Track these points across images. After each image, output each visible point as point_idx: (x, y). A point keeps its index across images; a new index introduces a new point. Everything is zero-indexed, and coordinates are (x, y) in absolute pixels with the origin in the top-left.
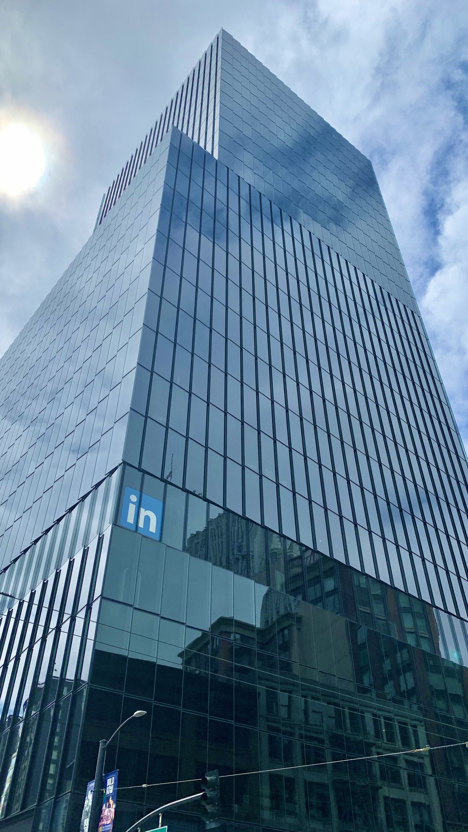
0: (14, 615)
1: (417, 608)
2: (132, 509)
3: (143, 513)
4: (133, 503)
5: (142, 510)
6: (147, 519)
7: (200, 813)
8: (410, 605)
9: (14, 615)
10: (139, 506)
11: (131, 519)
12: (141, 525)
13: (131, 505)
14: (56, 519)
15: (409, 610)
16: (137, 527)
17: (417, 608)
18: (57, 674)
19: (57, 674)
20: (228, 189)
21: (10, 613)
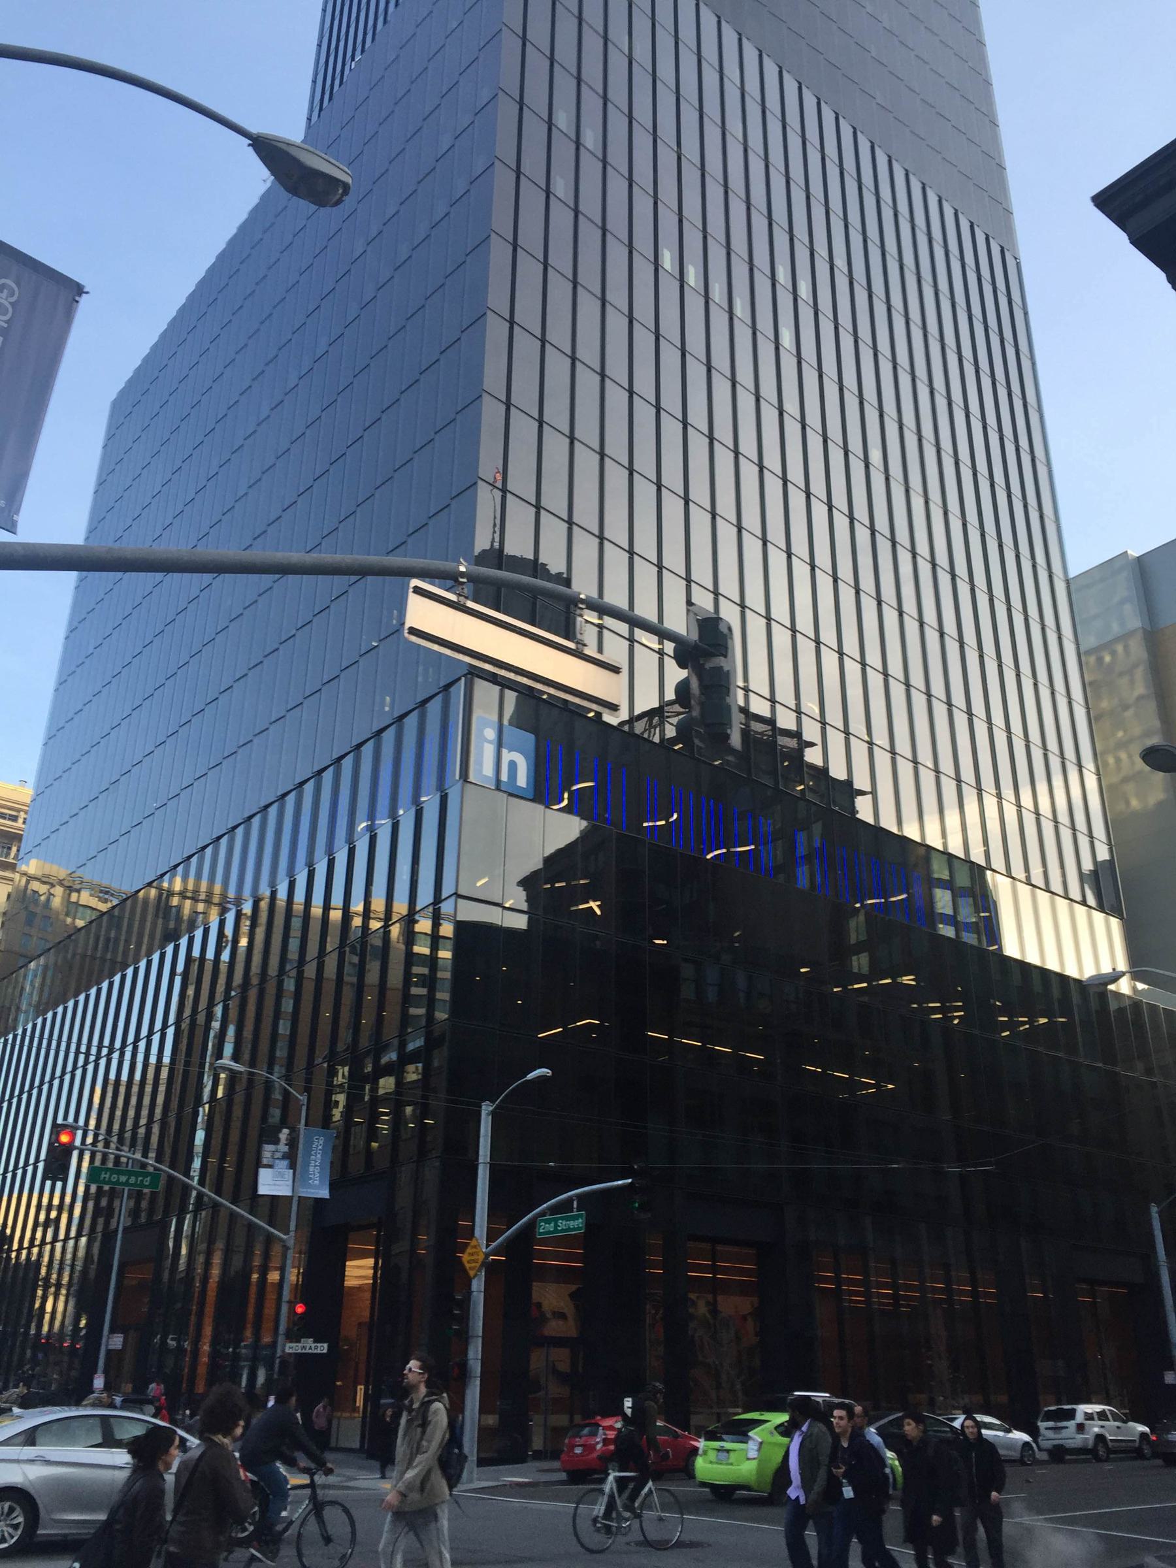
0: (28, 1033)
1: (963, 880)
2: (489, 751)
3: (507, 756)
4: (490, 742)
5: (504, 751)
6: (513, 765)
7: (1103, 854)
8: (951, 876)
9: (28, 1033)
10: (500, 745)
11: (488, 770)
12: (504, 777)
13: (486, 745)
14: (279, 794)
15: (948, 885)
16: (498, 781)
17: (963, 880)
18: (59, 1184)
19: (59, 1184)
20: (631, 253)
21: (25, 1031)
